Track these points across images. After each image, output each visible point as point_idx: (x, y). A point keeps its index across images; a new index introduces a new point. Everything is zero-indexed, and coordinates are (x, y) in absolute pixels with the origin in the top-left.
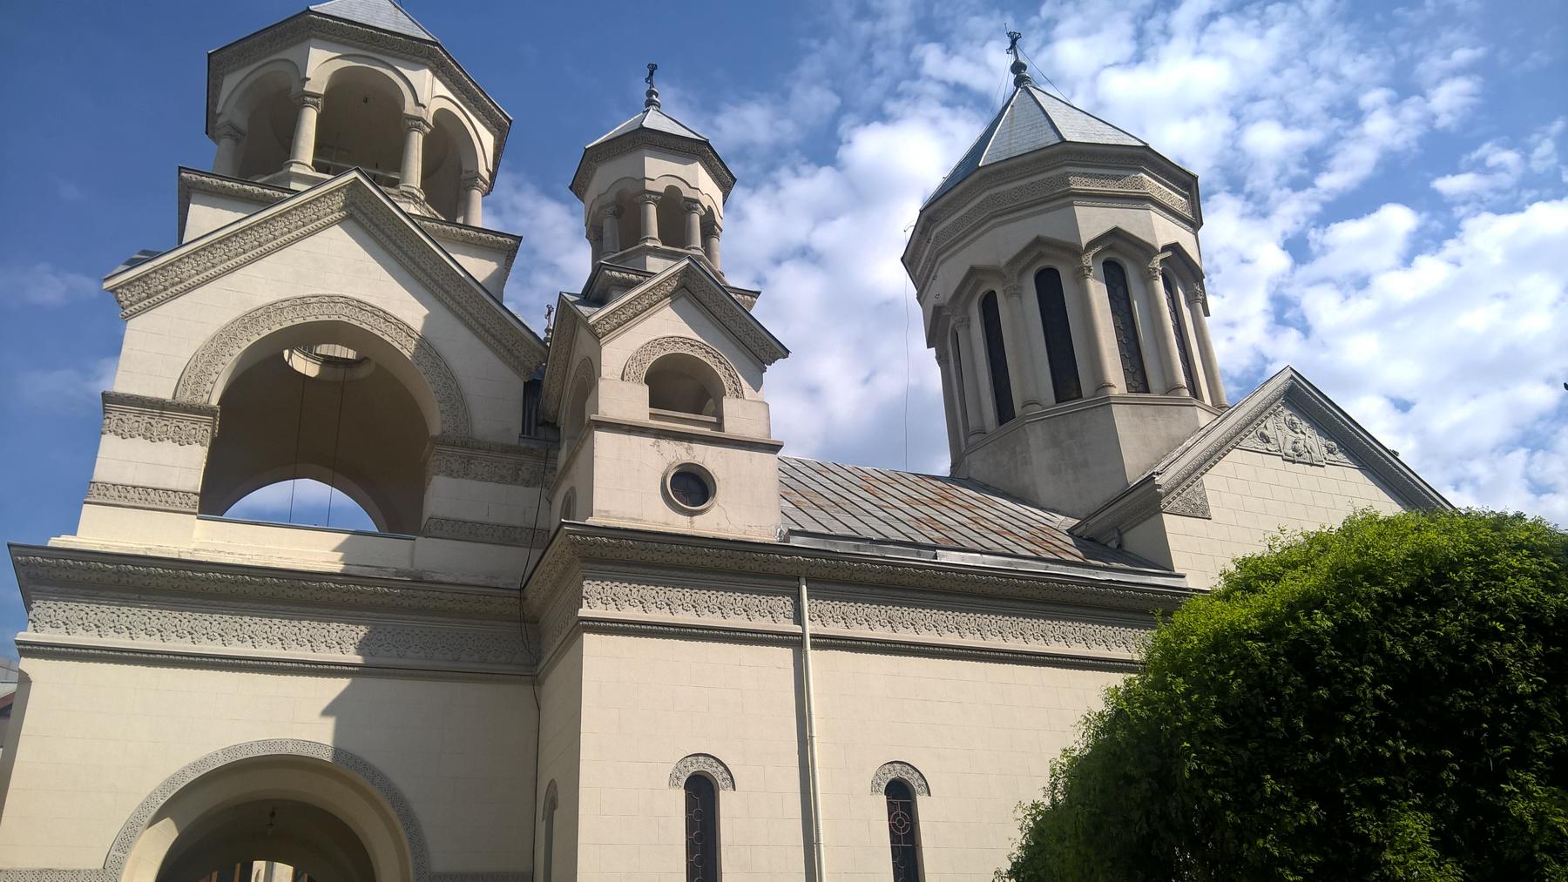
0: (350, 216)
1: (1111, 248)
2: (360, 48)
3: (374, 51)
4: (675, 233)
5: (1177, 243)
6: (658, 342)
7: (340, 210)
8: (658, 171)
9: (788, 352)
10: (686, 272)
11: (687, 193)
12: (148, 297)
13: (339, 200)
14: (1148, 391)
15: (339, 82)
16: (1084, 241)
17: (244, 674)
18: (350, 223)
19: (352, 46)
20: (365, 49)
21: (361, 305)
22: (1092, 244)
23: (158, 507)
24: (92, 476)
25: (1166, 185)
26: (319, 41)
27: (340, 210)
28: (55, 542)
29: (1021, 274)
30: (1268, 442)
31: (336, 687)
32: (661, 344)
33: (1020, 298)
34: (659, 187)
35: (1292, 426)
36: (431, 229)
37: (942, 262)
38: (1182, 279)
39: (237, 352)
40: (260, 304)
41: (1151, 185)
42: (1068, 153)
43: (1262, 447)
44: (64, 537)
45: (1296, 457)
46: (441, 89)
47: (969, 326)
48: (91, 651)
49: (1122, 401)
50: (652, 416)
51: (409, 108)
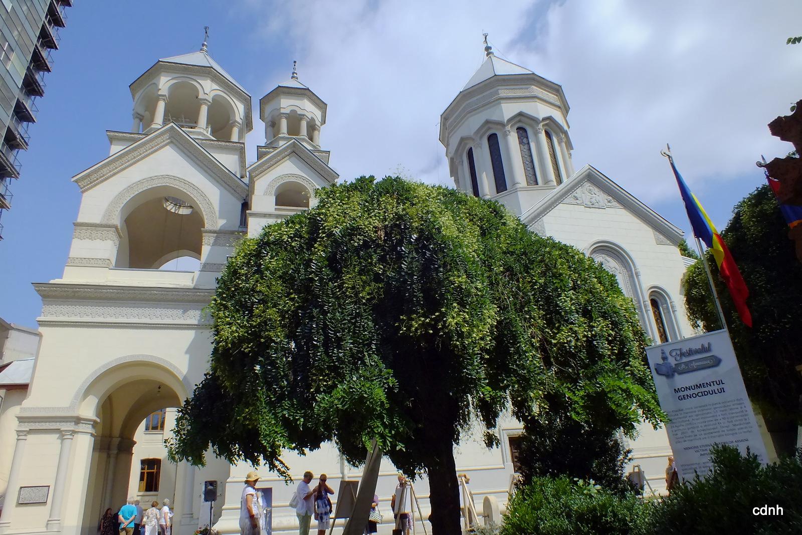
0: (172, 142)
1: (520, 121)
2: (181, 74)
3: (187, 74)
4: (294, 130)
5: (551, 116)
6: (281, 177)
7: (169, 139)
8: (286, 104)
9: (339, 175)
10: (294, 144)
11: (300, 112)
12: (91, 183)
13: (167, 136)
14: (537, 184)
15: (173, 89)
16: (506, 118)
17: (100, 329)
18: (172, 145)
19: (178, 73)
20: (184, 74)
21: (175, 178)
22: (510, 120)
23: (78, 265)
24: (68, 255)
25: (546, 90)
26: (165, 73)
27: (169, 139)
28: (52, 282)
29: (481, 137)
30: (577, 199)
31: (191, 334)
32: (282, 178)
33: (481, 148)
34: (287, 111)
35: (590, 191)
36: (202, 143)
37: (450, 137)
38: (554, 132)
39: (119, 209)
40: (134, 181)
41: (536, 90)
42: (498, 80)
43: (574, 202)
44: (57, 280)
45: (591, 206)
46: (215, 87)
47: (463, 165)
48: (64, 323)
49: (523, 189)
50: (276, 209)
51: (201, 96)
